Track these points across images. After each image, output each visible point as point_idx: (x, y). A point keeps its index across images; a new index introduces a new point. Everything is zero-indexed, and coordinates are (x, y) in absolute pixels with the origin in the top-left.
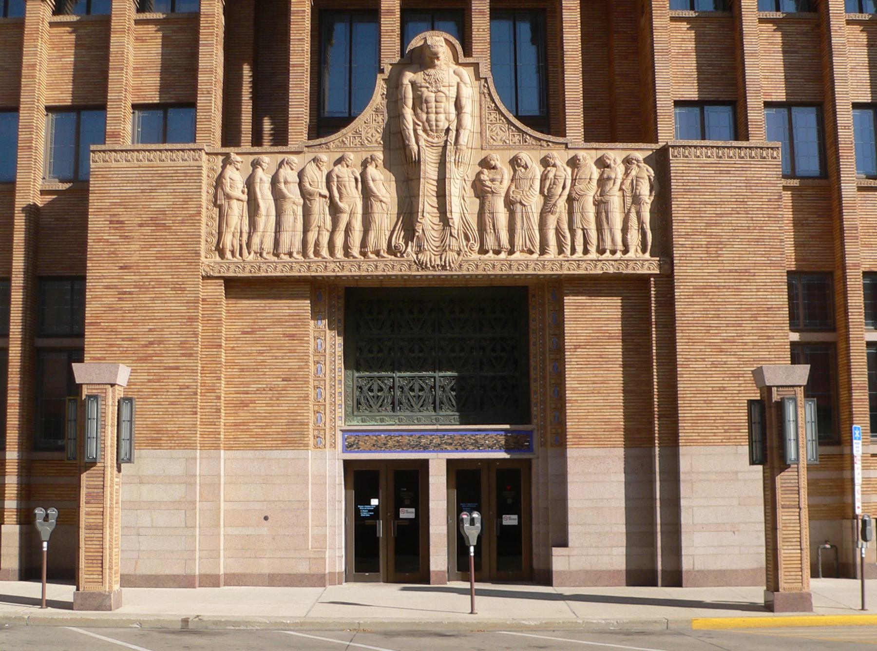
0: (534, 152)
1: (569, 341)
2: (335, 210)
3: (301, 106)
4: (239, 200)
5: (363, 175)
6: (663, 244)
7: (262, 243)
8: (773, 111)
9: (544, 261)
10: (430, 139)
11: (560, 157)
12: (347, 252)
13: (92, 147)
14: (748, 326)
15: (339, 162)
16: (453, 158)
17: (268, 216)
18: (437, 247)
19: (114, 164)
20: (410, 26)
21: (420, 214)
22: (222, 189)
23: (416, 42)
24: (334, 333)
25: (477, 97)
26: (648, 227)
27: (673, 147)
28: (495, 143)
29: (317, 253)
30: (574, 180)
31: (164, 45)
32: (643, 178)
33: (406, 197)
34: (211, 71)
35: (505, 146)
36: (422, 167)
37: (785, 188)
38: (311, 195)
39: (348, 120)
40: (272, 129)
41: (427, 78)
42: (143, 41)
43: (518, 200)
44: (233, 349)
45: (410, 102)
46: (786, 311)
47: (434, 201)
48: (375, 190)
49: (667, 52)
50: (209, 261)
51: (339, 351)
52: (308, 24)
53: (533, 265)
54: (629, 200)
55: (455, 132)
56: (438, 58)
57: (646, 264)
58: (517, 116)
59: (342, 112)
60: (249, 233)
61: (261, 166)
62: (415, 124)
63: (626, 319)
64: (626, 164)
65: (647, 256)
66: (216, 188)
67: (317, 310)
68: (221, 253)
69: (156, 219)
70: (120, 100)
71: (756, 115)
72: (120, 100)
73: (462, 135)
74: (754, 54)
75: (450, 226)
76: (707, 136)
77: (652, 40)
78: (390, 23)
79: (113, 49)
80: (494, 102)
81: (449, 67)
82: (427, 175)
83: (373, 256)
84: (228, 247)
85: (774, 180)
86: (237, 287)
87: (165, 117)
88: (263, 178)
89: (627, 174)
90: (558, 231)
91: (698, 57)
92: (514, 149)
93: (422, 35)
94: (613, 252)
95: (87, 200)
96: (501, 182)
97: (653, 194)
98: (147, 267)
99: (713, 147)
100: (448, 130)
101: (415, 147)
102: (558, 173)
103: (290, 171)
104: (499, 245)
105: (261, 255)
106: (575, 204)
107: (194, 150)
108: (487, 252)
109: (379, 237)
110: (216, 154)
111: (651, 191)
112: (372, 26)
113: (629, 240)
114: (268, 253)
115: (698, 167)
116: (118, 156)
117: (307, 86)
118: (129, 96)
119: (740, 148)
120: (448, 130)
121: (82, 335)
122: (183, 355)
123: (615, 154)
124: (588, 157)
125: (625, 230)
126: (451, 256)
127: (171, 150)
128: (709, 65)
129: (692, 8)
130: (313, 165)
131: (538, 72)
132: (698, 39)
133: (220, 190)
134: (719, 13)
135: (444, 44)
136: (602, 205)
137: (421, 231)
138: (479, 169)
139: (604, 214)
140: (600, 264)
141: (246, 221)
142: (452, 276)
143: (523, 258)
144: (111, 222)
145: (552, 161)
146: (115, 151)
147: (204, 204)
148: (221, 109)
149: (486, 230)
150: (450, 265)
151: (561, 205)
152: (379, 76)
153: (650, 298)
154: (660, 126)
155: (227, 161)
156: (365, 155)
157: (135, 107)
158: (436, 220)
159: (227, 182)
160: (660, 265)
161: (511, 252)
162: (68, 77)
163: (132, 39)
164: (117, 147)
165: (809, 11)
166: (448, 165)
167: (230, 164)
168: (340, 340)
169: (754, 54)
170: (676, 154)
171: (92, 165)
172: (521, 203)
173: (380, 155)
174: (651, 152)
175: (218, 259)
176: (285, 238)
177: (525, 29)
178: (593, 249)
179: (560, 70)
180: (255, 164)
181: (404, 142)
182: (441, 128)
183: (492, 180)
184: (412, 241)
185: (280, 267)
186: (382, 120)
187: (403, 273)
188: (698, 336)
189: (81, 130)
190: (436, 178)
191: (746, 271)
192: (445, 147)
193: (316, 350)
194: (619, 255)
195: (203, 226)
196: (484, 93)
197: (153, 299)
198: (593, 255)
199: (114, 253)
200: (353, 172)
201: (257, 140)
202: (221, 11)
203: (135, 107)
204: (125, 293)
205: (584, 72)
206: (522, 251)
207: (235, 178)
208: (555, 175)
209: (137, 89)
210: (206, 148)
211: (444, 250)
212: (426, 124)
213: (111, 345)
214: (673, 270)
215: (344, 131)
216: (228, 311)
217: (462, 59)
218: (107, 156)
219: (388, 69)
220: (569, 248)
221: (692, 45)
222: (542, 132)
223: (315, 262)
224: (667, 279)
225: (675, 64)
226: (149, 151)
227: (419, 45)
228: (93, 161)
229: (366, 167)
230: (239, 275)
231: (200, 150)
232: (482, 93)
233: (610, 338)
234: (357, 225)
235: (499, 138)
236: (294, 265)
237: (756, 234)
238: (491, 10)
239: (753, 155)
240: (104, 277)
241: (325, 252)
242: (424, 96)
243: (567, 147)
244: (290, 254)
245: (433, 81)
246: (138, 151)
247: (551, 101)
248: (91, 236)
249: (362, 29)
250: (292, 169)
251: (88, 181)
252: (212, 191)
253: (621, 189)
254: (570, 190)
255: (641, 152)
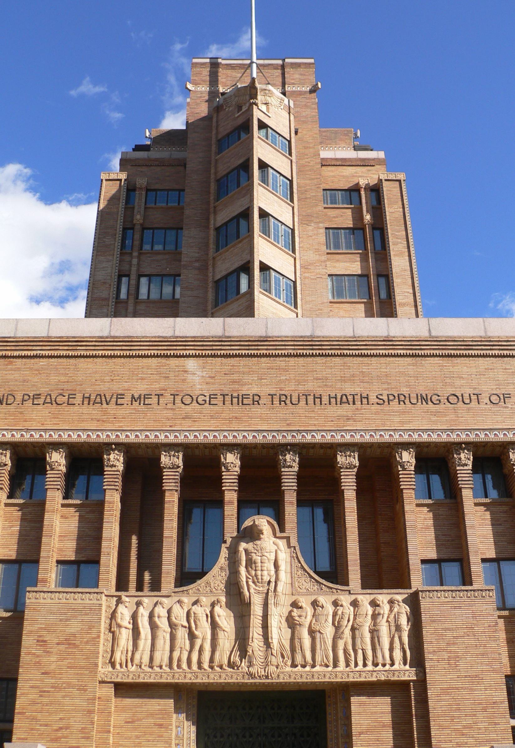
0: (328, 596)
1: (355, 729)
2: (192, 636)
3: (170, 565)
4: (126, 628)
5: (212, 612)
6: (418, 659)
7: (141, 659)
8: (487, 565)
9: (336, 672)
10: (257, 588)
11: (345, 600)
12: (200, 666)
13: (28, 589)
14: (481, 716)
15: (195, 603)
16: (273, 601)
17: (146, 639)
18: (262, 663)
19: (42, 601)
20: (245, 511)
21: (250, 639)
22: (115, 620)
23: (248, 523)
24: (190, 723)
25: (289, 559)
26: (407, 647)
27: (422, 591)
28: (301, 591)
29: (179, 666)
30: (355, 616)
31: (80, 522)
32: (402, 613)
33: (241, 628)
34: (110, 540)
35: (308, 593)
36: (252, 607)
37: (500, 617)
38: (176, 625)
39: (202, 574)
40: (150, 579)
41: (255, 546)
42: (66, 518)
43: (317, 629)
44: (118, 733)
45: (244, 563)
46: (506, 704)
47: (260, 631)
48: (219, 622)
49: (416, 527)
50: (104, 671)
51: (193, 736)
52: (176, 510)
53: (329, 675)
54: (393, 629)
55: (274, 583)
56: (262, 534)
57: (407, 673)
58: (315, 572)
59: (197, 569)
60: (133, 651)
61: (142, 605)
62: (247, 578)
63: (394, 712)
64: (390, 604)
65: (407, 667)
66: (111, 619)
67: (178, 706)
68: (113, 665)
69: (69, 640)
70: (49, 557)
71: (476, 567)
72: (49, 557)
73: (279, 585)
74: (473, 527)
75: (271, 648)
76: (444, 584)
77: (405, 520)
78: (231, 510)
79: (45, 523)
80: (300, 563)
81: (270, 539)
82: (255, 613)
83: (218, 669)
84: (118, 661)
85: (492, 612)
86: (123, 689)
87: (78, 570)
88: (144, 614)
89: (391, 610)
90: (345, 651)
91: (435, 530)
92: (314, 594)
93: (252, 518)
94: (384, 665)
95: (22, 624)
96: (306, 617)
97: (410, 624)
98: (61, 674)
99: (448, 591)
100: (269, 582)
101: (247, 594)
102: (344, 611)
103: (162, 609)
104: (305, 661)
105: (140, 667)
106: (357, 632)
107: (97, 593)
108: (296, 666)
109: (222, 656)
110: (113, 596)
111: (408, 622)
112: (217, 511)
113: (394, 656)
114: (145, 666)
115: (438, 604)
116: (46, 595)
117: (175, 551)
118: (55, 555)
119: (467, 591)
120: (269, 582)
121: (12, 721)
122: (83, 738)
123: (383, 597)
124: (365, 599)
125: (391, 649)
126: (272, 669)
127: (82, 593)
128: (443, 535)
129: (430, 498)
130: (178, 605)
131: (329, 541)
132: (435, 518)
133: (113, 621)
134: (448, 501)
135: (266, 524)
136: (375, 633)
137: (251, 652)
138: (291, 608)
139: (376, 638)
140: (375, 674)
141: (131, 643)
142: (272, 683)
143: (322, 670)
144: (38, 641)
145: (340, 603)
146: (44, 592)
147: (102, 630)
148: (116, 565)
149: (295, 651)
150: (271, 676)
151: (347, 633)
152: (223, 545)
153: (411, 697)
154: (412, 577)
155: (119, 601)
156: (213, 599)
157: (58, 562)
158: (262, 644)
159: (119, 615)
160: (416, 673)
161: (313, 666)
162: (15, 540)
163: (59, 516)
164: (45, 589)
165: (507, 497)
166: (269, 606)
167: (122, 603)
168: (194, 729)
169: (473, 527)
170: (424, 596)
171: (28, 601)
172: (319, 632)
173: (223, 599)
174: (407, 595)
175: (110, 669)
176: (158, 655)
177: (319, 513)
178: (369, 663)
179: (344, 541)
180: (138, 604)
181: (239, 590)
182: (264, 580)
183: (300, 616)
184: (245, 658)
185: (153, 675)
186: (224, 575)
187: (239, 681)
188: (446, 724)
189: (21, 577)
190: (261, 615)
191: (476, 676)
192: (267, 594)
193: (177, 736)
194: (388, 667)
195: (101, 646)
196: (293, 557)
197: (64, 697)
198: (370, 667)
199: (38, 662)
200: (205, 611)
201: (140, 588)
202: (119, 500)
203: (58, 562)
204: (44, 692)
205: (360, 541)
206: (321, 665)
207: (124, 614)
208: (342, 612)
209: (60, 550)
210: (105, 592)
211: (267, 665)
212: (255, 578)
213: (32, 729)
214: (426, 677)
215: (199, 582)
216: (116, 706)
217: (278, 534)
218: (38, 595)
219: (229, 540)
220: (353, 663)
221: (431, 522)
222: (332, 582)
223: (178, 673)
224: (422, 683)
225: (421, 535)
226: (67, 592)
227: (250, 524)
228: (28, 599)
229: (214, 607)
230: (125, 681)
231: (102, 593)
232: (292, 557)
233: (384, 726)
234: (207, 647)
235: (304, 587)
236: (163, 674)
237: (481, 650)
238: (298, 501)
239: (476, 595)
240: (31, 680)
241: (184, 666)
242: (254, 559)
243: (350, 593)
244: (161, 667)
245: (259, 548)
246: (59, 592)
247: (338, 562)
248: (23, 651)
249: (212, 513)
250: (163, 608)
251: (24, 612)
252: (108, 621)
253: (387, 621)
254: (353, 623)
255: (400, 596)
